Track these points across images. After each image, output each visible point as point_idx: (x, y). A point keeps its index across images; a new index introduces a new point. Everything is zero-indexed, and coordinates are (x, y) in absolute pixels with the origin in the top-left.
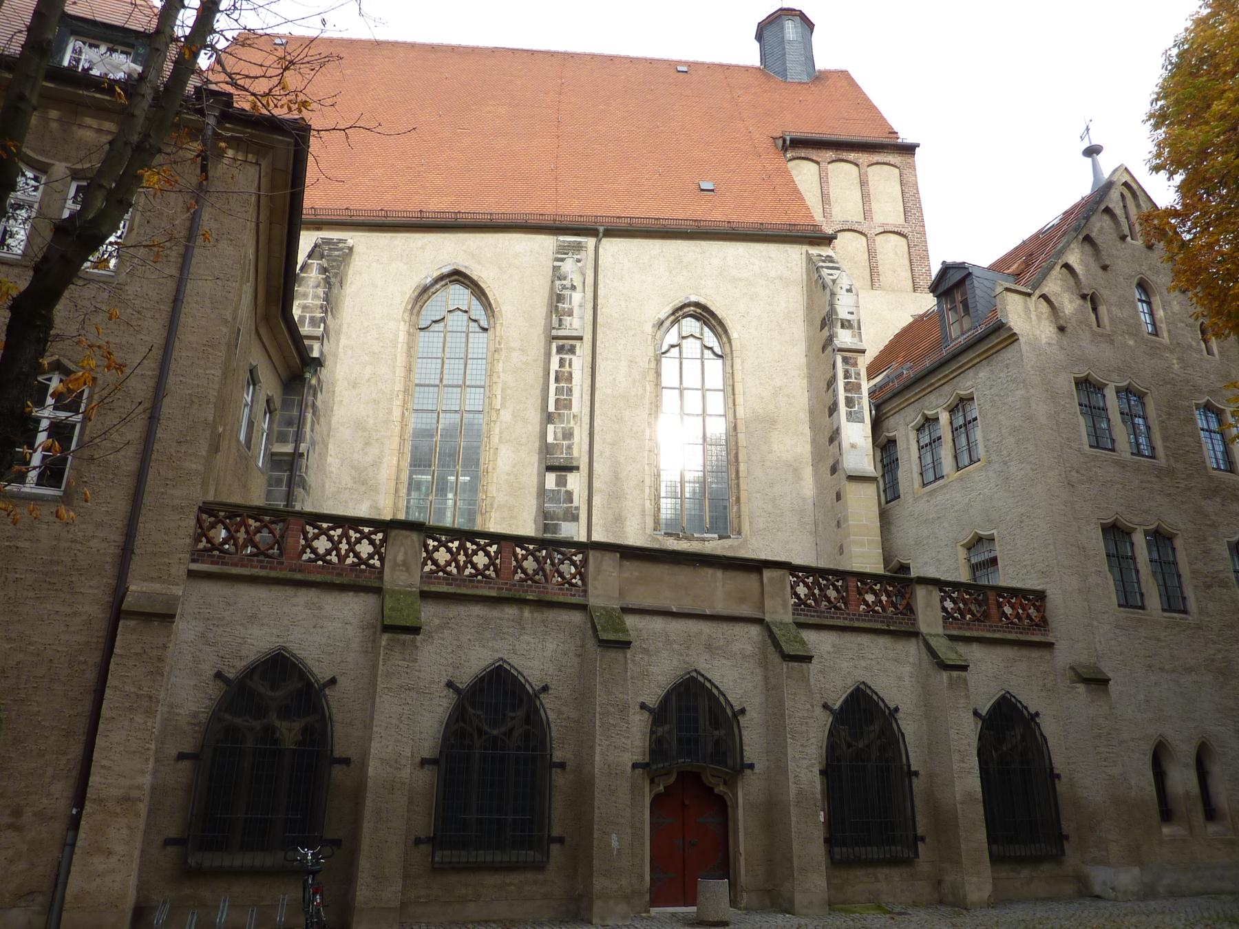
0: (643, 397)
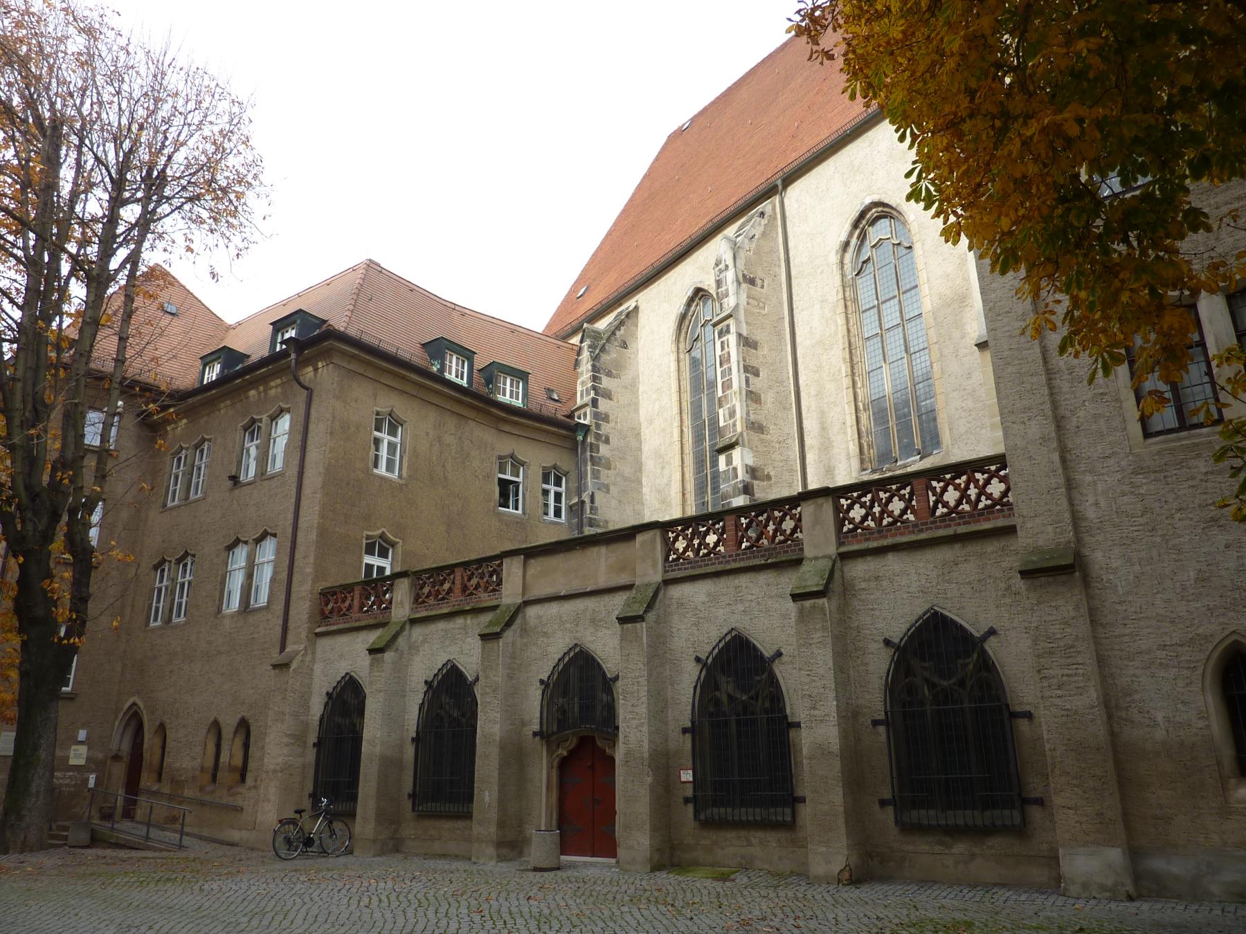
0: (836, 332)
